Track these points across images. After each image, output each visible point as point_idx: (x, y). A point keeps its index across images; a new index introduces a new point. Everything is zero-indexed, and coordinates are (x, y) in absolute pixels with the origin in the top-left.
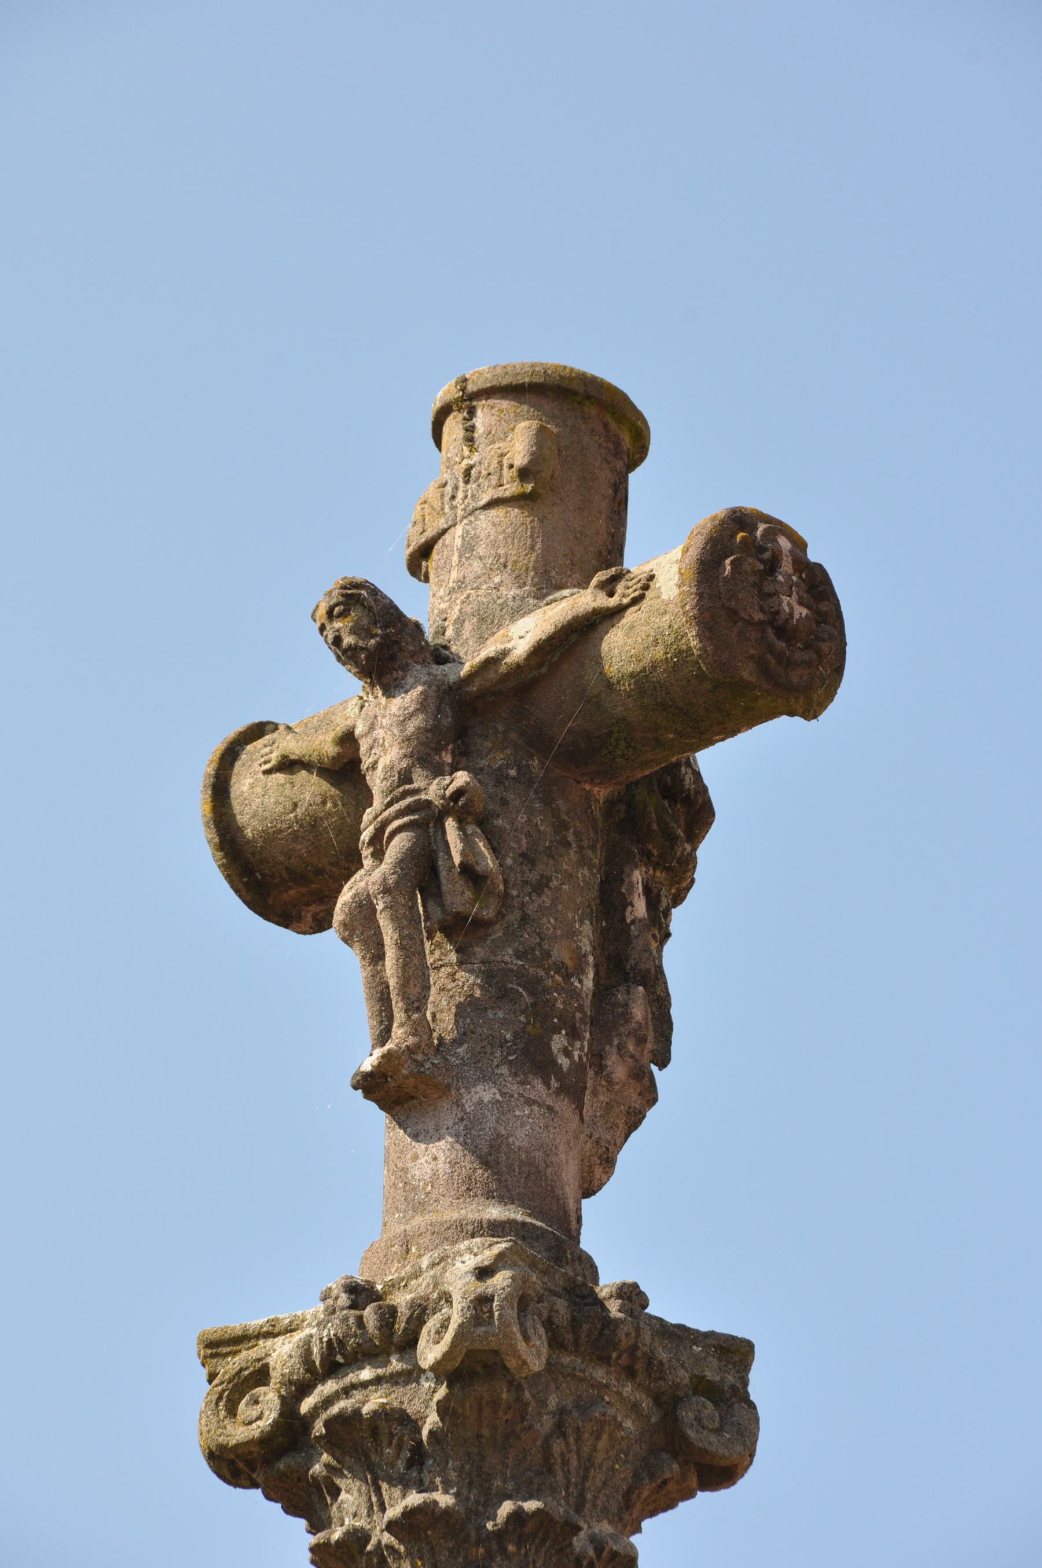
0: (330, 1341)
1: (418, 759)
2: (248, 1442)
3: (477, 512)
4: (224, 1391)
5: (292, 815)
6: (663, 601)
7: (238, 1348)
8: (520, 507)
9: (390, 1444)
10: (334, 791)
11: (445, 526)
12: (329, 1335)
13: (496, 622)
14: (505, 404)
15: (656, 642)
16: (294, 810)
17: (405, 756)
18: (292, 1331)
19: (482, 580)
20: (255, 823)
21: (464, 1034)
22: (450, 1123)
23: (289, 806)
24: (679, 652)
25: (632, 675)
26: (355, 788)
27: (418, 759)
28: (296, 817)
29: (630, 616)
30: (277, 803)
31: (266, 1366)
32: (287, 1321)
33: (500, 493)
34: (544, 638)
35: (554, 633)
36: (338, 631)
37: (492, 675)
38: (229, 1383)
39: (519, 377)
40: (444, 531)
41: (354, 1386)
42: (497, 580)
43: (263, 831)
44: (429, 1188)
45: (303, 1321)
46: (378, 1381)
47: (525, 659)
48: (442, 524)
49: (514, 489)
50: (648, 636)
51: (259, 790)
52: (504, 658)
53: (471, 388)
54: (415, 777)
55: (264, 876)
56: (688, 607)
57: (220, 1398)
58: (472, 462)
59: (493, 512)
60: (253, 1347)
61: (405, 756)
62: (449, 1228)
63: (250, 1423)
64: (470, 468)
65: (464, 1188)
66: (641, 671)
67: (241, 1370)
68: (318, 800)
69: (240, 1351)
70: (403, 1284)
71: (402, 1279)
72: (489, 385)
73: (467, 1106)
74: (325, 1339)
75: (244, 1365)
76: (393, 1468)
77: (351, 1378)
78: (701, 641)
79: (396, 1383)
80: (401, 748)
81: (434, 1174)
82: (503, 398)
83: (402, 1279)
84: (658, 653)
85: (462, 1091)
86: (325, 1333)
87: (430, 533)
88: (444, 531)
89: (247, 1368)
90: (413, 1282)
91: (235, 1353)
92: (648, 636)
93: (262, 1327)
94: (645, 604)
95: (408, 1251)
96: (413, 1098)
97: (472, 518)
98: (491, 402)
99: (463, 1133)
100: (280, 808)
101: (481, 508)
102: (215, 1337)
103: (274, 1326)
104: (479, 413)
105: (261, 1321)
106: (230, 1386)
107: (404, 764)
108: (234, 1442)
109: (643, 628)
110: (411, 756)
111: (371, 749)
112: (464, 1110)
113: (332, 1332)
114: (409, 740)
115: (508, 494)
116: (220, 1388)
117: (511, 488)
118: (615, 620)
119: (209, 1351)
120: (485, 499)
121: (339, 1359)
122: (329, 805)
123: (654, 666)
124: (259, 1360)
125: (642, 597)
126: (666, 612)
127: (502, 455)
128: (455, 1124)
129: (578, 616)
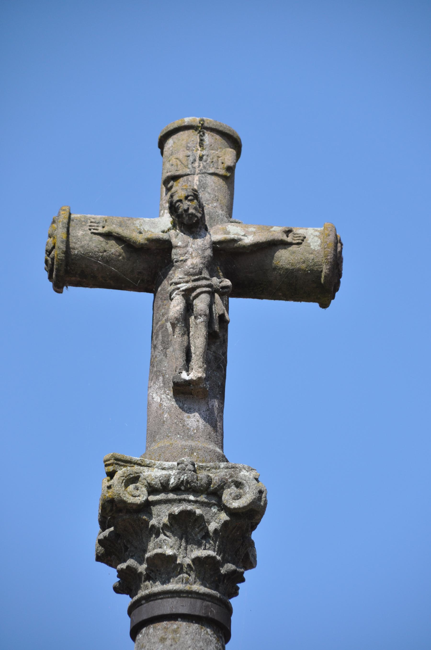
0: (183, 481)
2: (135, 504)
3: (206, 174)
4: (124, 480)
5: (101, 254)
6: (311, 249)
8: (223, 180)
9: (198, 528)
11: (189, 173)
12: (183, 478)
14: (218, 137)
15: (304, 262)
16: (103, 253)
17: (202, 263)
18: (149, 467)
19: (210, 202)
20: (81, 250)
22: (204, 410)
23: (102, 250)
25: (287, 269)
27: (206, 266)
28: (102, 255)
29: (294, 248)
30: (96, 247)
31: (139, 477)
32: (148, 462)
33: (217, 171)
37: (231, 245)
38: (126, 477)
40: (188, 175)
41: (184, 500)
42: (215, 204)
44: (195, 431)
45: (154, 465)
46: (196, 502)
50: (302, 259)
51: (88, 238)
54: (203, 272)
56: (329, 257)
57: (122, 482)
58: (204, 154)
59: (213, 177)
60: (133, 467)
61: (202, 263)
63: (135, 497)
64: (203, 156)
65: (208, 437)
66: (292, 270)
67: (130, 474)
68: (117, 254)
70: (208, 469)
71: (208, 467)
72: (214, 127)
73: (210, 405)
75: (131, 473)
77: (184, 496)
78: (329, 271)
79: (203, 506)
80: (201, 259)
82: (217, 134)
83: (208, 467)
84: (303, 266)
87: (178, 173)
88: (188, 175)
90: (213, 470)
91: (125, 466)
92: (302, 259)
93: (138, 461)
94: (302, 246)
95: (192, 453)
96: (191, 394)
97: (203, 175)
98: (212, 133)
100: (97, 249)
102: (119, 457)
104: (206, 135)
106: (126, 479)
107: (201, 266)
108: (130, 502)
111: (186, 254)
112: (209, 407)
113: (186, 478)
114: (205, 257)
115: (220, 173)
116: (123, 478)
117: (222, 172)
118: (286, 247)
120: (211, 171)
121: (183, 488)
122: (120, 258)
124: (137, 473)
125: (301, 244)
126: (312, 253)
128: (206, 411)
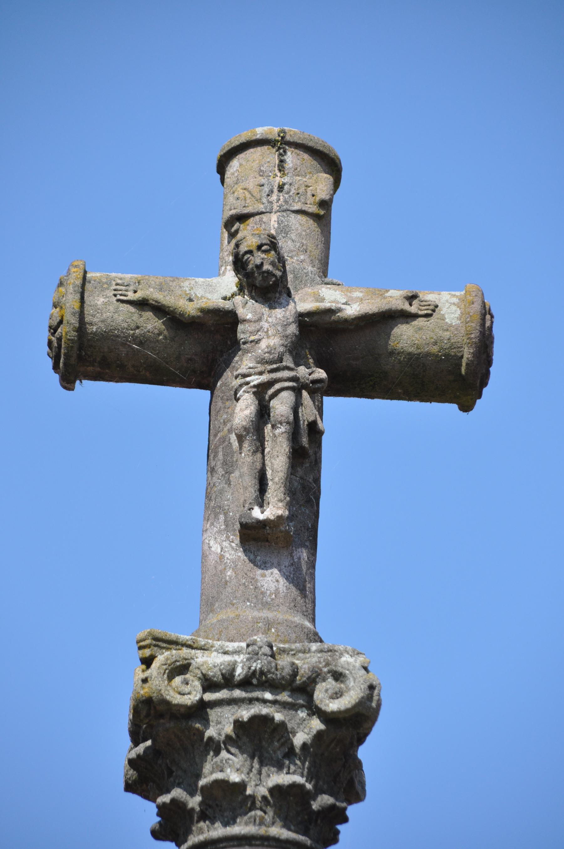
0: (255, 671)
1: (289, 349)
4: (166, 669)
5: (132, 332)
6: (447, 323)
7: (170, 646)
8: (314, 220)
10: (166, 332)
11: (264, 210)
12: (256, 667)
13: (303, 282)
14: (306, 156)
15: (435, 343)
16: (135, 330)
17: (283, 345)
19: (294, 253)
20: (101, 325)
21: (293, 515)
22: (287, 564)
24: (448, 355)
25: (410, 354)
26: (186, 336)
27: (289, 349)
28: (134, 334)
31: (189, 665)
33: (305, 208)
34: (370, 313)
35: (377, 313)
36: (263, 259)
37: (326, 318)
38: (169, 666)
39: (317, 145)
42: (302, 257)
43: (105, 332)
44: (273, 596)
45: (212, 647)
46: (274, 702)
47: (352, 319)
48: (261, 208)
49: (314, 209)
52: (337, 313)
53: (288, 138)
54: (285, 358)
55: (86, 354)
56: (473, 336)
57: (164, 673)
58: (285, 181)
59: (299, 217)
61: (283, 345)
62: (296, 626)
66: (417, 354)
67: (176, 661)
68: (156, 331)
69: (171, 649)
70: (293, 653)
71: (292, 650)
72: (301, 142)
74: (253, 668)
75: (178, 659)
76: (275, 754)
78: (473, 357)
79: (285, 708)
81: (277, 590)
83: (292, 650)
85: (294, 548)
86: (254, 665)
89: (178, 661)
91: (167, 649)
93: (187, 641)
94: (432, 320)
95: (269, 629)
96: (267, 541)
99: (293, 572)
100: (125, 325)
101: (291, 211)
102: (160, 636)
103: (194, 643)
104: (289, 153)
105: (188, 637)
106: (170, 668)
107: (282, 349)
109: (429, 332)
110: (286, 347)
112: (293, 559)
113: (259, 666)
114: (287, 337)
117: (313, 209)
118: (409, 320)
119: (154, 642)
120: (296, 207)
121: (255, 681)
122: (161, 337)
123: (428, 354)
124: (186, 659)
126: (447, 330)
127: (307, 186)
128: (289, 566)
129: (391, 309)
